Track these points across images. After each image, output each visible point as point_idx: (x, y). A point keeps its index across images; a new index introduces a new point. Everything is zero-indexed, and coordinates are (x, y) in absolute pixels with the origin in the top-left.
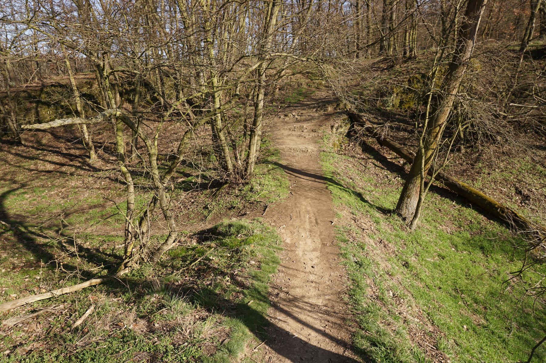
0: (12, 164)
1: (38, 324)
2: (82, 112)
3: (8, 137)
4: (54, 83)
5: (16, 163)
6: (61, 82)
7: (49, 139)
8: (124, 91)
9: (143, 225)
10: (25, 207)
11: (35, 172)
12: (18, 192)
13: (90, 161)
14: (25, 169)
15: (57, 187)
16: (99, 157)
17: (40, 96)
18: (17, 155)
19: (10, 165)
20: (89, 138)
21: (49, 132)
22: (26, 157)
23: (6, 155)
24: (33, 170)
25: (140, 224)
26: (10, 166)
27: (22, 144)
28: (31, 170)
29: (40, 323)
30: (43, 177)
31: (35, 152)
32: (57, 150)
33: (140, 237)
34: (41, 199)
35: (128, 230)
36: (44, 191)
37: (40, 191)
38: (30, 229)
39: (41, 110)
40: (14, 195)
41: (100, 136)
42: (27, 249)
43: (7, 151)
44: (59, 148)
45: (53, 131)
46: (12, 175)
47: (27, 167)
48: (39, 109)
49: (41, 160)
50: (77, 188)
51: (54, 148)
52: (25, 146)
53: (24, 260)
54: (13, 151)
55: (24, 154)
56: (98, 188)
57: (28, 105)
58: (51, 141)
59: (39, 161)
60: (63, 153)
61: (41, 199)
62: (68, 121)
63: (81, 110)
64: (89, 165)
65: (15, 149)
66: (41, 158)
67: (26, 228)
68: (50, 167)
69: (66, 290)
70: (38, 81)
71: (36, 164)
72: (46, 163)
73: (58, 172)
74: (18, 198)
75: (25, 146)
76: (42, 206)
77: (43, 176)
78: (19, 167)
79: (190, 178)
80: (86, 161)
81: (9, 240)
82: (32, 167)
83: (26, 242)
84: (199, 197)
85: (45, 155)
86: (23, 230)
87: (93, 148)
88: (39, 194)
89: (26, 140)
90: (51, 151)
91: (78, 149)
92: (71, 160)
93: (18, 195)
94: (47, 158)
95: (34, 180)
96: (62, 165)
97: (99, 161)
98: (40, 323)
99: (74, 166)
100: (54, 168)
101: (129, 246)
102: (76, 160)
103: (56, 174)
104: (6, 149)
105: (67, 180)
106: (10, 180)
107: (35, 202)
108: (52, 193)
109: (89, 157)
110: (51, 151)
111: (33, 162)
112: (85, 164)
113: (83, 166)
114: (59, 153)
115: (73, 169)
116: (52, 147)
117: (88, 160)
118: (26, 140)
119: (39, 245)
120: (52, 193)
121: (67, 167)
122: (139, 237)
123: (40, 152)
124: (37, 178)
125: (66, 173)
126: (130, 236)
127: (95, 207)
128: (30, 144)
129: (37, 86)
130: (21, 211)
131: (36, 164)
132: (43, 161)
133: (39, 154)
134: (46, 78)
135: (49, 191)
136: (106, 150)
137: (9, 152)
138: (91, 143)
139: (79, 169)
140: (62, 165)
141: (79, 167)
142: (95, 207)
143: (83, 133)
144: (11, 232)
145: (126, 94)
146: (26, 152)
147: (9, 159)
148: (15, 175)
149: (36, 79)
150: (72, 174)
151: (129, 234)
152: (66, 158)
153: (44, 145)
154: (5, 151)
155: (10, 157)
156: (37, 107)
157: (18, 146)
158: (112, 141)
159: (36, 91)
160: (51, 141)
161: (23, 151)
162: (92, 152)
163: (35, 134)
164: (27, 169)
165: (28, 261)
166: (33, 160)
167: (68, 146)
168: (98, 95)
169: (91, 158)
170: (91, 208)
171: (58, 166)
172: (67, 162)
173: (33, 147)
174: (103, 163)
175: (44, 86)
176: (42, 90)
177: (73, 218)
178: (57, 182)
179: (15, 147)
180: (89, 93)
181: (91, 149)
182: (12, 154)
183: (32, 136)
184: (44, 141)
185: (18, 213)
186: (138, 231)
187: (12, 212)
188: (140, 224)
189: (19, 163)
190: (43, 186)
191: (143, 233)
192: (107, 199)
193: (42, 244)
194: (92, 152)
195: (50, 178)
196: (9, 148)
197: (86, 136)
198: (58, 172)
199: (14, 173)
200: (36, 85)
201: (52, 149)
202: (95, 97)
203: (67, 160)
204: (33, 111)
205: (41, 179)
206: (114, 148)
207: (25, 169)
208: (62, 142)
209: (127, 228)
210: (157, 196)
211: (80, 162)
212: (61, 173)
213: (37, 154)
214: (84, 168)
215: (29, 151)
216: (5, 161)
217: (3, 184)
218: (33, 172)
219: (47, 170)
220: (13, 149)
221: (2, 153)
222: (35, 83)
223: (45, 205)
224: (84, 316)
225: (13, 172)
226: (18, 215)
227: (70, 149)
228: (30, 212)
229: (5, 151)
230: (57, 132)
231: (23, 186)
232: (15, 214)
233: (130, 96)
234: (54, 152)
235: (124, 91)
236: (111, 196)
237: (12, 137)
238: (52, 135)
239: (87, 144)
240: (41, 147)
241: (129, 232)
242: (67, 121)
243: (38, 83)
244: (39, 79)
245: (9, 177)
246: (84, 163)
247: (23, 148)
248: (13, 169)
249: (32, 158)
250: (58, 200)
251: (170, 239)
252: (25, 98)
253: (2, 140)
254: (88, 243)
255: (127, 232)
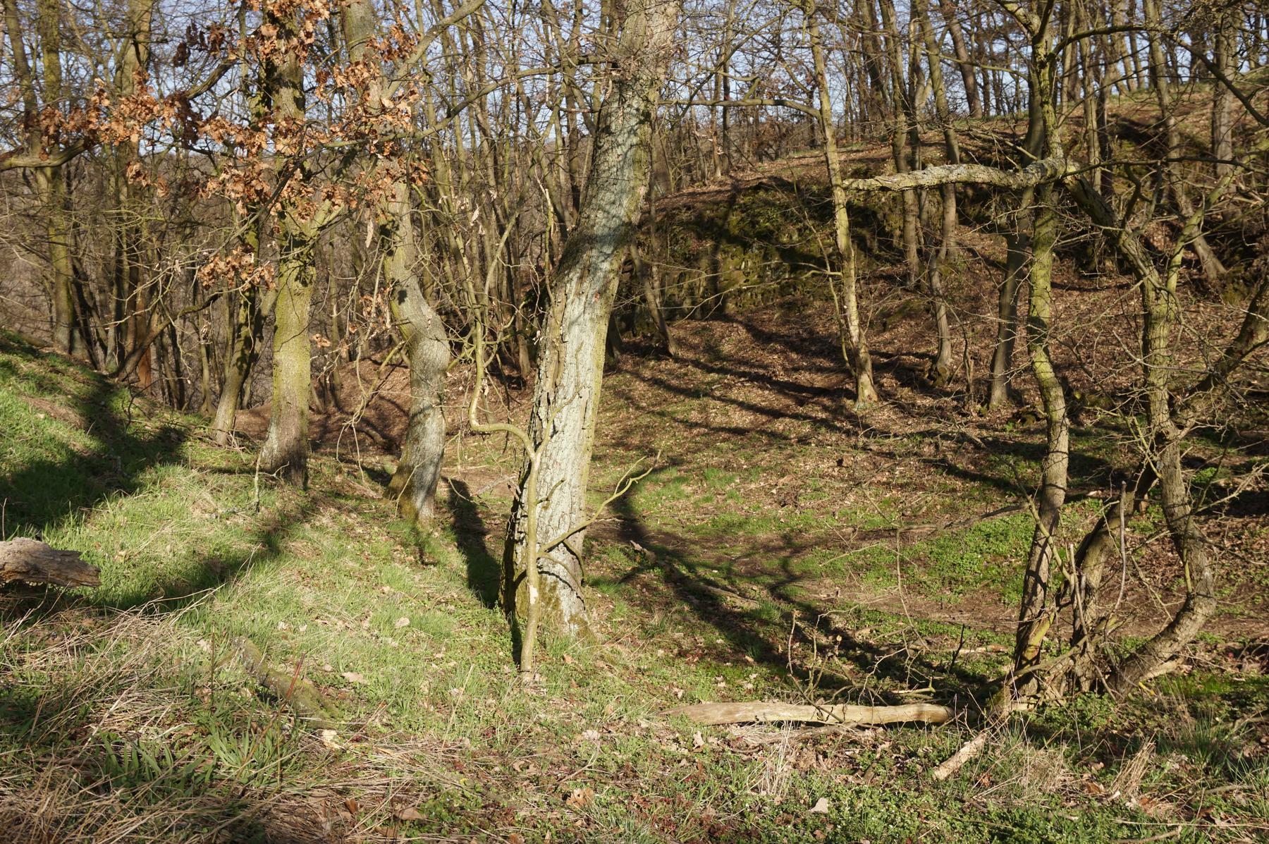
0: (643, 408)
1: (821, 757)
2: (850, 254)
3: (635, 336)
4: (764, 181)
5: (654, 405)
6: (785, 176)
7: (740, 341)
8: (970, 192)
9: (1091, 562)
10: (684, 515)
11: (703, 430)
12: (663, 476)
13: (857, 408)
14: (675, 420)
15: (764, 470)
16: (884, 395)
17: (726, 216)
18: (655, 382)
19: (638, 408)
20: (860, 335)
21: (741, 323)
22: (678, 391)
23: (630, 381)
24: (696, 425)
25: (1081, 556)
26: (638, 413)
27: (670, 355)
28: (691, 425)
29: (825, 756)
30: (724, 445)
31: (700, 376)
32: (761, 371)
33: (1079, 599)
34: (725, 500)
35: (1036, 574)
36: (731, 480)
37: (720, 479)
38: (701, 571)
39: (724, 259)
40: (656, 482)
41: (887, 335)
42: (701, 618)
43: (631, 373)
44: (765, 367)
45: (750, 320)
46: (644, 435)
47: (680, 417)
48: (719, 257)
49: (719, 399)
50: (822, 477)
51: (752, 366)
52: (677, 360)
53: (701, 640)
54: (647, 374)
55: (674, 382)
56: (884, 483)
57: (693, 243)
58: (744, 348)
59: (712, 403)
60: (778, 383)
61: (725, 500)
62: (959, 171)
63: (848, 249)
64: (852, 418)
65: (651, 368)
66: (718, 393)
67: (691, 567)
68: (741, 419)
69: (853, 712)
70: (723, 178)
71: (703, 409)
72: (731, 408)
73: (762, 432)
74: (665, 491)
75: (677, 360)
76: (728, 518)
77: (724, 440)
78: (662, 414)
79: (1208, 473)
80: (843, 407)
81: (656, 589)
82: (695, 416)
83: (695, 601)
84: (1252, 534)
85: (729, 387)
86: (684, 571)
87: (869, 366)
88: (718, 486)
89: (680, 342)
90: (743, 374)
91: (820, 370)
92: (801, 403)
93: (665, 484)
94: (734, 394)
95: (699, 450)
96: (775, 414)
97: (882, 408)
98: (825, 756)
99: (810, 418)
100: (752, 423)
101: (1035, 628)
102: (816, 403)
103: (759, 440)
104: (629, 367)
105: (792, 456)
106: (638, 448)
107: (710, 506)
108: (753, 486)
109: (854, 396)
110: (743, 374)
111: (695, 402)
112: (842, 414)
113: (835, 419)
114: (764, 381)
115: (806, 429)
116: (745, 362)
117: (849, 402)
118: (680, 342)
119: (731, 613)
120: (753, 486)
121: (787, 420)
122: (1072, 602)
123: (715, 376)
124: (707, 446)
125: (786, 438)
126: (1041, 595)
127: (877, 534)
128: (690, 355)
129: (719, 192)
130: (674, 527)
131: (703, 409)
132: (723, 401)
133: (713, 382)
134: (743, 170)
135: (744, 480)
136: (908, 376)
137: (637, 375)
138: (863, 354)
139: (823, 430)
140: (775, 414)
141: (823, 422)
142: (877, 534)
143: (845, 318)
144: (657, 570)
145: (973, 201)
146: (678, 377)
147: (636, 394)
148: (652, 435)
149: (719, 174)
150: (803, 441)
151: (1039, 587)
152: (785, 395)
153: (725, 359)
154: (627, 371)
155: (640, 388)
156: (716, 249)
157: (659, 359)
158: (923, 350)
159: (717, 203)
160: (744, 348)
161: (671, 372)
162: (865, 379)
163: (704, 328)
164: (681, 421)
165: (711, 647)
166: (698, 397)
167: (792, 361)
168: (887, 209)
169: (860, 398)
170: (864, 536)
171: (764, 418)
172: (788, 406)
173: (696, 364)
174: (895, 413)
175: (737, 189)
176: (732, 201)
177: (813, 561)
178: (766, 458)
179: (653, 363)
180: (862, 204)
181: (862, 369)
182: (643, 380)
183: (696, 333)
184: (727, 348)
185: (667, 529)
186: (1073, 579)
187: (652, 525)
188: (1081, 556)
189: (660, 404)
190: (727, 467)
191: (1088, 590)
192: (913, 517)
193: (739, 613)
194: (865, 379)
195: (743, 447)
196: (636, 364)
197: (854, 330)
198: (762, 432)
199: (648, 430)
200: (716, 188)
201: (747, 370)
202: (880, 216)
203: (789, 402)
204: (704, 262)
205: (718, 449)
206: (931, 370)
207: (675, 420)
208: (774, 351)
209: (1033, 568)
210: (1155, 464)
211: (825, 409)
212: (773, 435)
213: (708, 383)
214: (839, 425)
215: (686, 374)
216: (627, 399)
217: (623, 457)
218: (695, 431)
219: (733, 426)
220: (647, 367)
221: (620, 377)
222: (713, 182)
223: (737, 517)
224: (955, 758)
225: (647, 427)
226: (667, 534)
227: (796, 370)
228: (696, 530)
229: (627, 371)
230: (763, 321)
231: (675, 462)
232: (660, 532)
233: (988, 208)
234: (753, 378)
235: (970, 192)
236: (924, 509)
237: (644, 336)
238: (748, 331)
239: (854, 354)
240: (718, 364)
241: (1038, 580)
242: (955, 173)
243: (722, 183)
244: (725, 173)
245: (636, 440)
246: (838, 412)
247: (672, 365)
248: (646, 420)
249: (695, 394)
250: (768, 507)
251: (1186, 622)
252: (685, 225)
253: (621, 343)
254: (866, 632)
255: (1032, 580)
